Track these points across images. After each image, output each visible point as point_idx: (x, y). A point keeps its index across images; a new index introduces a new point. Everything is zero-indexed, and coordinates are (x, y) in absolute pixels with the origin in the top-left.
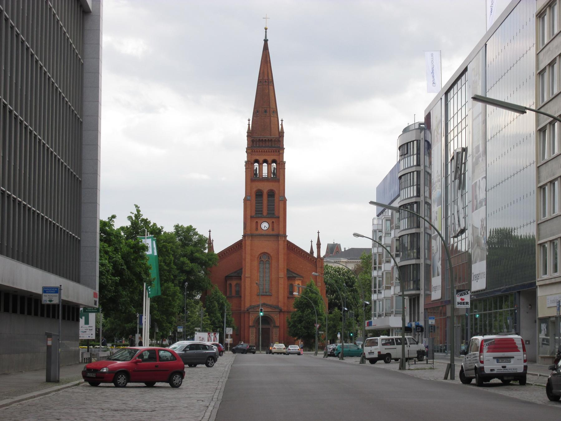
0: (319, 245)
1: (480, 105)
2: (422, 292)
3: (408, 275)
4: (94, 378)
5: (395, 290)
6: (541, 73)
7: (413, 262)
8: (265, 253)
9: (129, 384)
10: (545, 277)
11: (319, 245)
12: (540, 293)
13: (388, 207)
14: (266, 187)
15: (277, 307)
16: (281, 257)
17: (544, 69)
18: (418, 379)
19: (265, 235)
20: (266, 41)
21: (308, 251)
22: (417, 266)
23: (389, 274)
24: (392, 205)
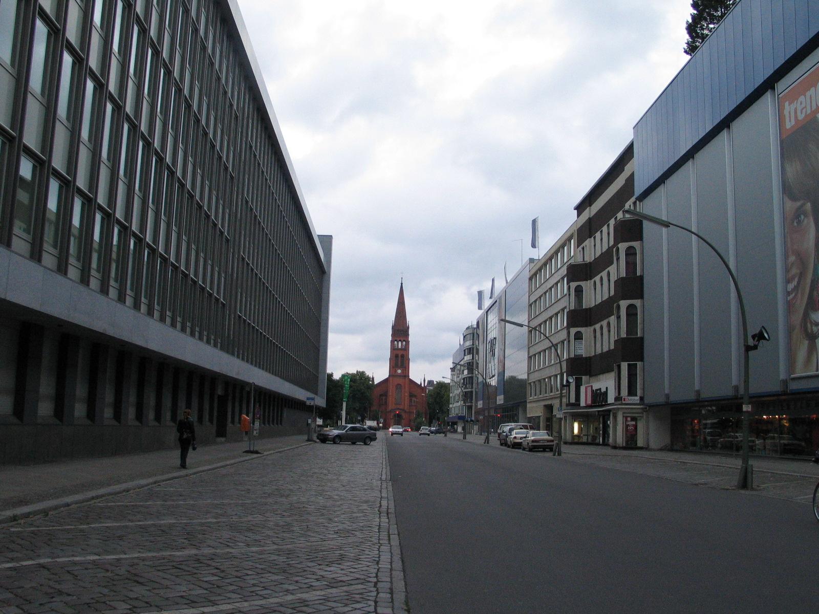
0: (424, 381)
1: (503, 323)
2: (474, 404)
3: (467, 396)
4: (324, 439)
5: (461, 403)
6: (530, 305)
7: (470, 390)
8: (398, 384)
9: (341, 443)
10: (531, 398)
11: (424, 381)
12: (528, 405)
13: (458, 364)
14: (400, 353)
15: (403, 410)
16: (407, 386)
17: (532, 303)
18: (403, 561)
19: (399, 376)
20: (402, 284)
21: (420, 384)
22: (472, 392)
23: (459, 395)
24: (460, 363)
